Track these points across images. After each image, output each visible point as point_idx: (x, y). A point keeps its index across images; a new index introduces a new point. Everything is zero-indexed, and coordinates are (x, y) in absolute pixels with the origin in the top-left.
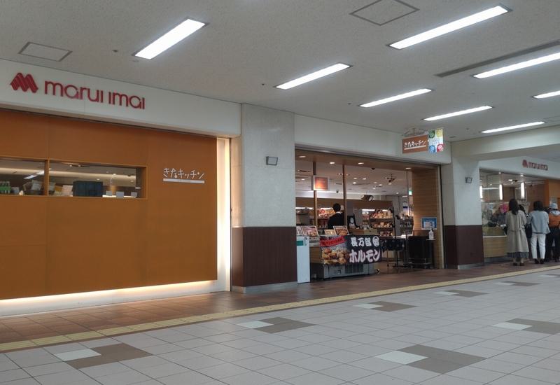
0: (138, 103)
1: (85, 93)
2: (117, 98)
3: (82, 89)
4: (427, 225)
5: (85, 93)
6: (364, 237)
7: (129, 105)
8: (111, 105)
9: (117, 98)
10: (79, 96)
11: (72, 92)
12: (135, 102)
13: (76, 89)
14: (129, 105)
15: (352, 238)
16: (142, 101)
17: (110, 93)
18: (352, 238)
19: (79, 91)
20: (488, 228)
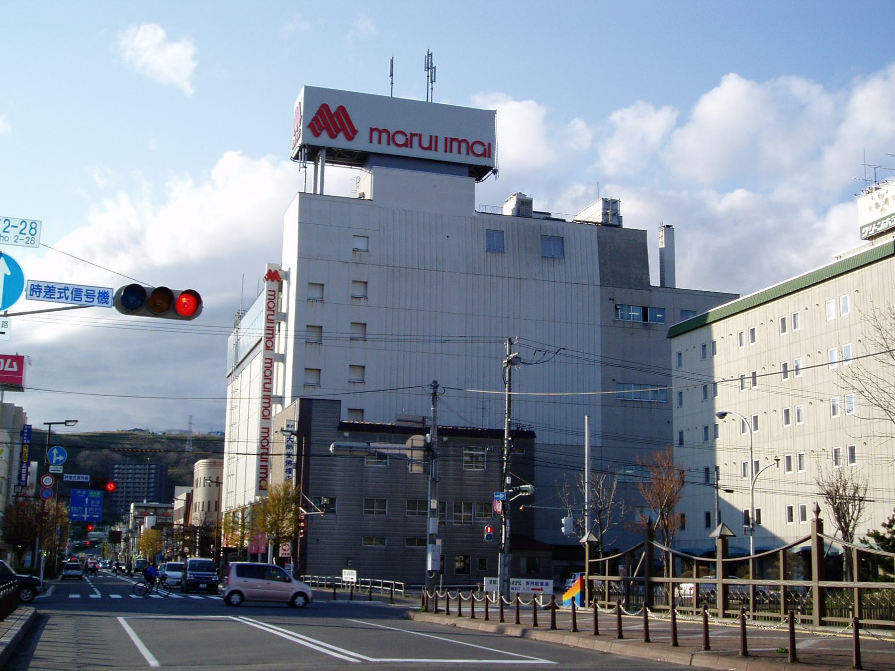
3: (412, 135)
10: (408, 144)
16: (487, 147)
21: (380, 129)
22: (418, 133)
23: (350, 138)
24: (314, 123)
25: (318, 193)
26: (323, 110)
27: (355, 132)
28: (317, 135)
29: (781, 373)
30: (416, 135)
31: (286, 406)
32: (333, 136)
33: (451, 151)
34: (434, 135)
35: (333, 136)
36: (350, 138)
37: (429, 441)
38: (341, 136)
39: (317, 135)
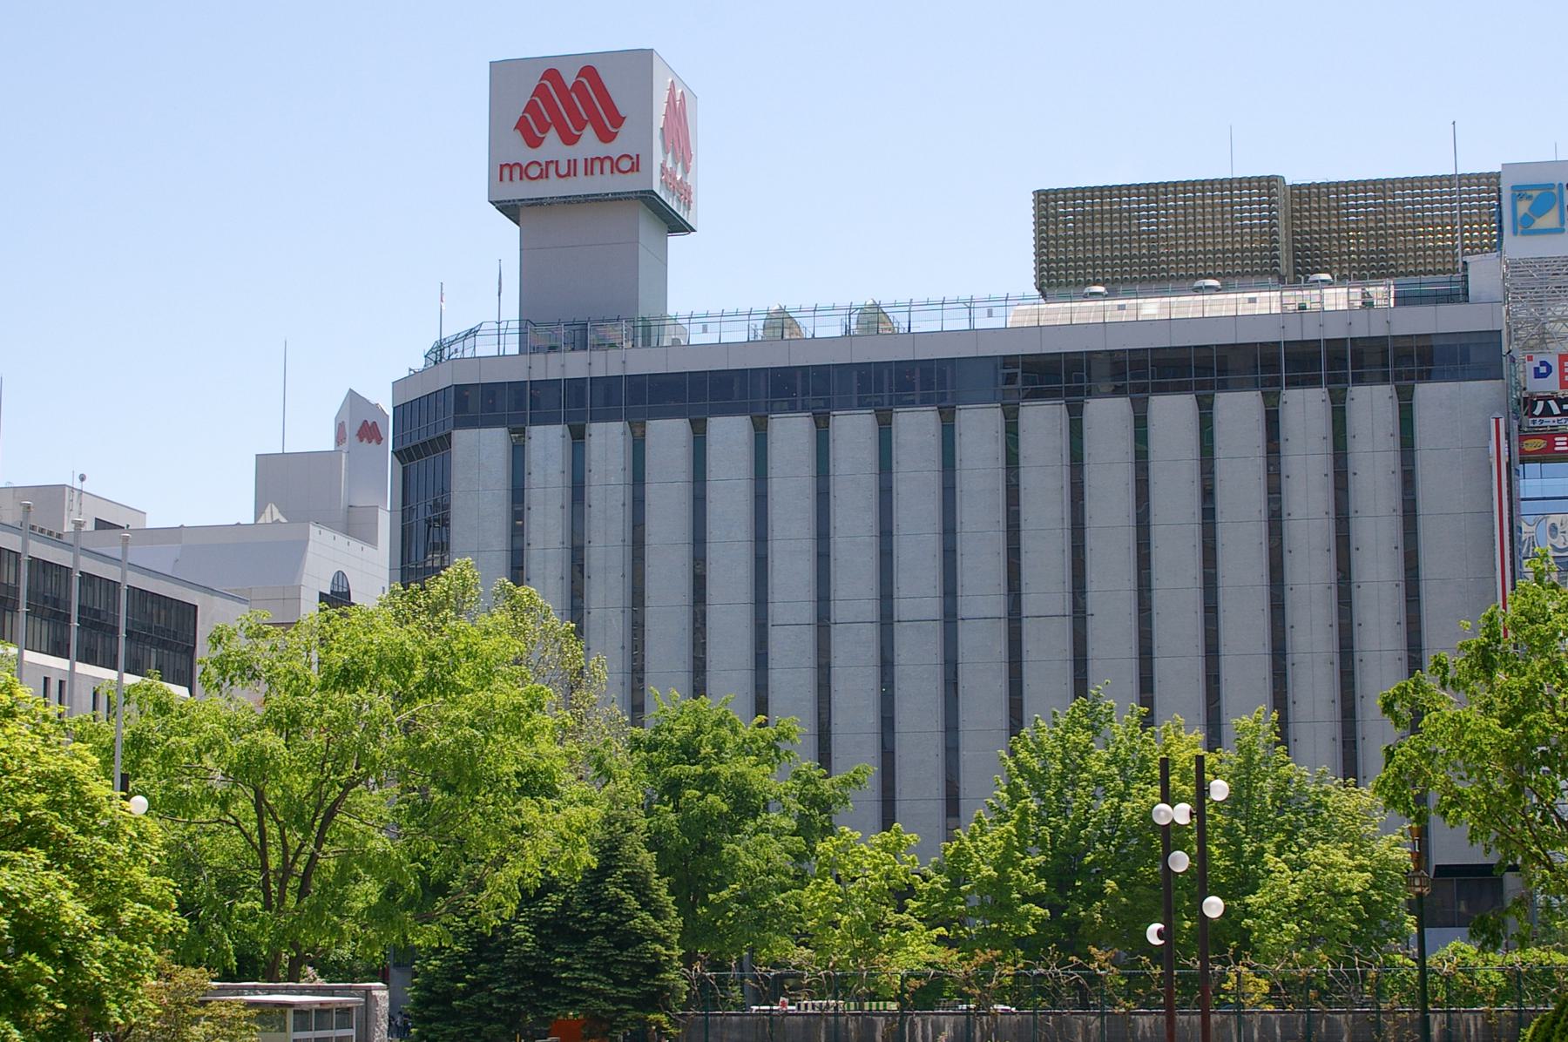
0: (539, 172)
1: (552, 168)
2: (597, 165)
3: (548, 163)
4: (1261, 751)
5: (552, 168)
6: (885, 1000)
7: (615, 171)
8: (589, 177)
9: (597, 165)
10: (544, 175)
11: (534, 171)
12: (625, 164)
13: (540, 165)
14: (615, 171)
15: (464, 440)
16: (635, 160)
17: (586, 160)
18: (464, 440)
19: (544, 167)
20: (1500, 676)
21: (511, 164)
22: (555, 160)
23: (606, 136)
24: (528, 115)
25: (501, 354)
26: (537, 99)
27: (618, 120)
28: (534, 142)
29: (1065, 616)
30: (552, 162)
31: (259, 522)
32: (569, 139)
33: (592, 173)
34: (572, 159)
35: (569, 139)
36: (606, 136)
37: (354, 732)
38: (589, 133)
39: (534, 142)
